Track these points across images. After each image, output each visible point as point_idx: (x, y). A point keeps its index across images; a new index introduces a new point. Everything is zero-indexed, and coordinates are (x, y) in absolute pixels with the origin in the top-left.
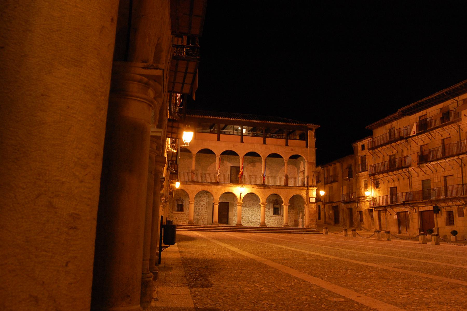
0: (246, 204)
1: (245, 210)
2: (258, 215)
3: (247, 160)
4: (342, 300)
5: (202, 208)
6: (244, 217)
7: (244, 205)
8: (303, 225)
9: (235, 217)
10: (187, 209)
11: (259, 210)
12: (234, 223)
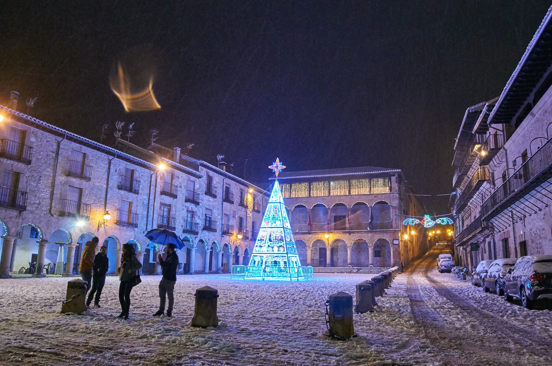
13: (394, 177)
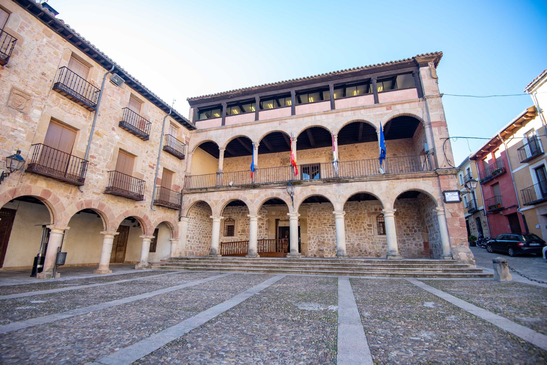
0: (328, 220)
1: (328, 229)
2: (350, 236)
3: (325, 153)
4: (524, 342)
5: (260, 229)
6: (327, 241)
7: (324, 221)
8: (5, 358)
9: (310, 242)
10: (239, 232)
11: (351, 229)
12: (310, 251)
13: (426, 68)
